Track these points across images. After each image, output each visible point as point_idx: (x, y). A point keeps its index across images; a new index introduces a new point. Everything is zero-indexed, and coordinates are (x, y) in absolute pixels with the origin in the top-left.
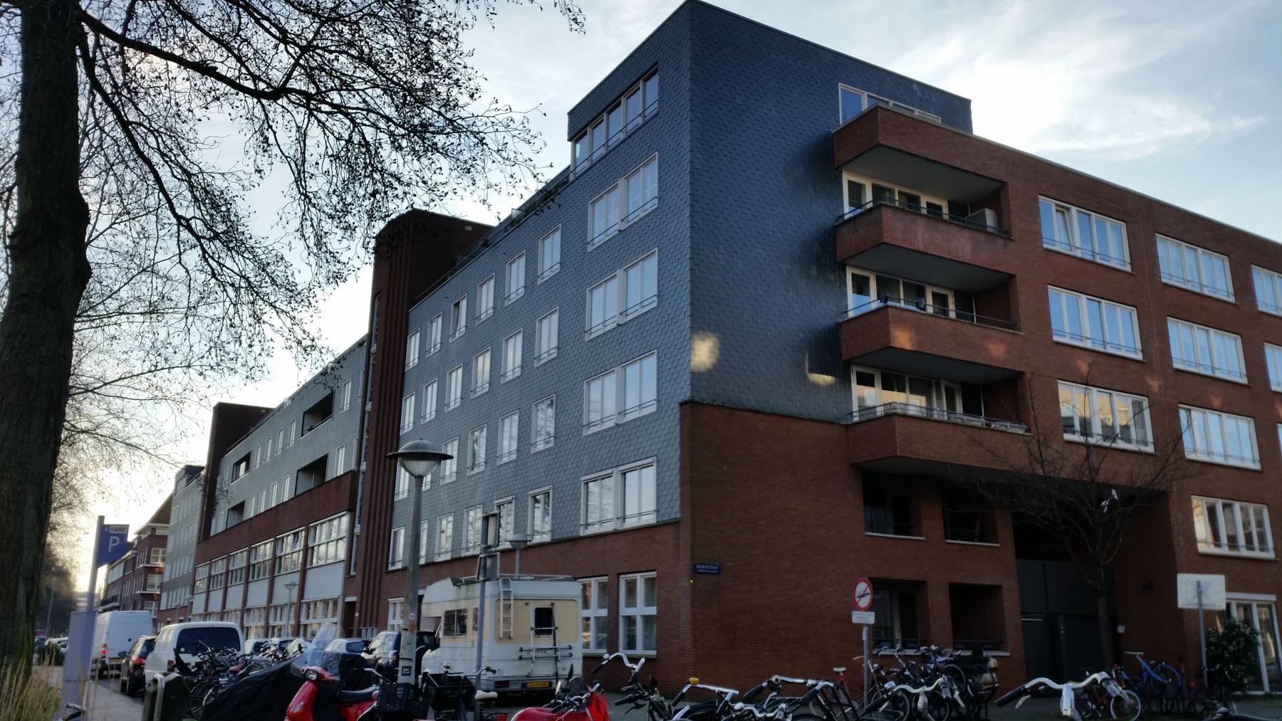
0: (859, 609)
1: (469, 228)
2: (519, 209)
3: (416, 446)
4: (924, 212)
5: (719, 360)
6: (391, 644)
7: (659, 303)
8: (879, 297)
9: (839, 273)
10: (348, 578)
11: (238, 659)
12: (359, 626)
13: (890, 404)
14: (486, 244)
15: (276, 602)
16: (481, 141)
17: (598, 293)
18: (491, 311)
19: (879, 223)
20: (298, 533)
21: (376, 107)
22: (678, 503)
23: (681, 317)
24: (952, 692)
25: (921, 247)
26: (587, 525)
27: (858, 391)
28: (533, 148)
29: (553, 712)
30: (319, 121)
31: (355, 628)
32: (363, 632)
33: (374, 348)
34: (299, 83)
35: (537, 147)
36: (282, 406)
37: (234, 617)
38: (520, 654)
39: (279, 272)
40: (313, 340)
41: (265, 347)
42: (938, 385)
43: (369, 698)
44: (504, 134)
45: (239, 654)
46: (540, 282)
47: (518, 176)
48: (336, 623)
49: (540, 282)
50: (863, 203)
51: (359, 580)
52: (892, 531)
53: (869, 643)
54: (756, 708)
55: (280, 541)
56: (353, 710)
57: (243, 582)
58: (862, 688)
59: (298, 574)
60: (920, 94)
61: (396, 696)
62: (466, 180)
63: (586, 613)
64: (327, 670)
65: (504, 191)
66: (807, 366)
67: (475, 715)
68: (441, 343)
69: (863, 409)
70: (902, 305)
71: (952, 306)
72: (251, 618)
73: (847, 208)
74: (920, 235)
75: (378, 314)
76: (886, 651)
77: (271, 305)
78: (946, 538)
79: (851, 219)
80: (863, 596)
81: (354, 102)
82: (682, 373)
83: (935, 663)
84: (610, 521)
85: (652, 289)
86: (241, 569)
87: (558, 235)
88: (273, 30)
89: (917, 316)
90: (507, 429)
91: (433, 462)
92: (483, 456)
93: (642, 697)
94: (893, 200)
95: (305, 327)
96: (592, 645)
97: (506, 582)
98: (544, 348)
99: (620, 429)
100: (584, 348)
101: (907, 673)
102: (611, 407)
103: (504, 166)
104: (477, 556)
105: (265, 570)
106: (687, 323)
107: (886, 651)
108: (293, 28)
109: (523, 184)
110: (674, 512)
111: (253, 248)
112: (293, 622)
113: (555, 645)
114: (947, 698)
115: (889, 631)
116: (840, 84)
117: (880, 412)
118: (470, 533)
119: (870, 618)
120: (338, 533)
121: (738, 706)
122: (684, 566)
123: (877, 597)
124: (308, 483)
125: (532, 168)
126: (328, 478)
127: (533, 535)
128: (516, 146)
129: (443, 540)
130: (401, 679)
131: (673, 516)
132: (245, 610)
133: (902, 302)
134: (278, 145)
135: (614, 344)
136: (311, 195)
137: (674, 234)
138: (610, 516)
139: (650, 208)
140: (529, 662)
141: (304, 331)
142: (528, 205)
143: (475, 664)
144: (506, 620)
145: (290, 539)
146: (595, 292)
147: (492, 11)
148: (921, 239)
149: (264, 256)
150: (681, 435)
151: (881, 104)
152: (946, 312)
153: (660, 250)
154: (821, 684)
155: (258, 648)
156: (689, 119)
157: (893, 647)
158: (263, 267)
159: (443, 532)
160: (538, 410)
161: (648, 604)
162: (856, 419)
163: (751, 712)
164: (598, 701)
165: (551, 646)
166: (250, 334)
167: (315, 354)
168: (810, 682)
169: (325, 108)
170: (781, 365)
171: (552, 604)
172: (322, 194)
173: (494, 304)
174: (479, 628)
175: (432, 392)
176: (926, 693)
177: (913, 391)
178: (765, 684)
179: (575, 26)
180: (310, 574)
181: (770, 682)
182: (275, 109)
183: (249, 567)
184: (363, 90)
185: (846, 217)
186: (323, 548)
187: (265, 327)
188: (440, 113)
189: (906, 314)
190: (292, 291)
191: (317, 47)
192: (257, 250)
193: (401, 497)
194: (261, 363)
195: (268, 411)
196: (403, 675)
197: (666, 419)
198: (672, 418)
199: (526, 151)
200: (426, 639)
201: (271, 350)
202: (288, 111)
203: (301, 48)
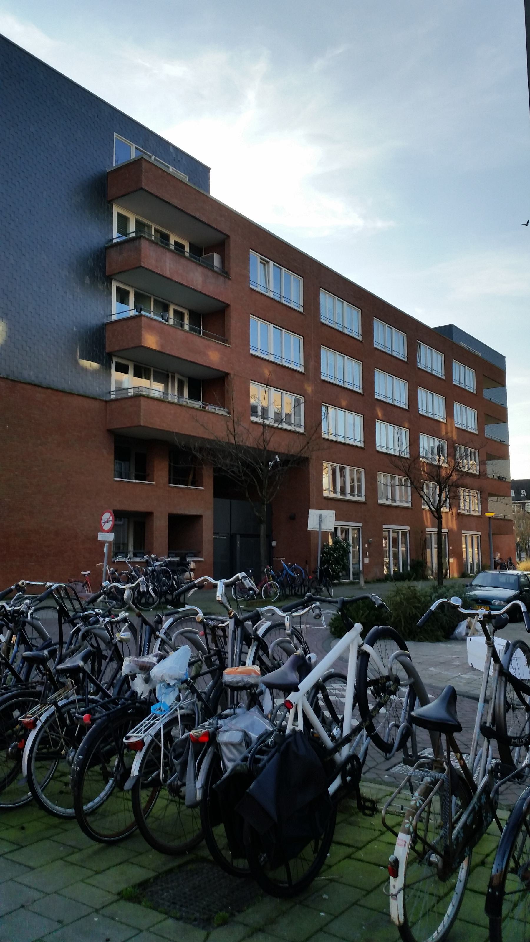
0: (104, 531)
4: (172, 247)
8: (136, 307)
9: (107, 285)
13: (139, 387)
19: (138, 250)
25: (168, 274)
27: (116, 375)
42: (173, 378)
52: (134, 478)
54: (8, 604)
60: (174, 156)
66: (78, 354)
69: (119, 389)
70: (152, 315)
73: (115, 234)
74: (168, 264)
76: (120, 559)
78: (170, 483)
79: (118, 244)
89: (162, 325)
94: (150, 235)
101: (133, 573)
107: (120, 559)
117: (131, 392)
119: (111, 537)
133: (152, 313)
148: (168, 268)
151: (145, 157)
152: (182, 326)
154: (56, 585)
162: (113, 397)
168: (48, 584)
176: (130, 588)
177: (156, 380)
178: (13, 587)
181: (18, 586)
189: (154, 323)
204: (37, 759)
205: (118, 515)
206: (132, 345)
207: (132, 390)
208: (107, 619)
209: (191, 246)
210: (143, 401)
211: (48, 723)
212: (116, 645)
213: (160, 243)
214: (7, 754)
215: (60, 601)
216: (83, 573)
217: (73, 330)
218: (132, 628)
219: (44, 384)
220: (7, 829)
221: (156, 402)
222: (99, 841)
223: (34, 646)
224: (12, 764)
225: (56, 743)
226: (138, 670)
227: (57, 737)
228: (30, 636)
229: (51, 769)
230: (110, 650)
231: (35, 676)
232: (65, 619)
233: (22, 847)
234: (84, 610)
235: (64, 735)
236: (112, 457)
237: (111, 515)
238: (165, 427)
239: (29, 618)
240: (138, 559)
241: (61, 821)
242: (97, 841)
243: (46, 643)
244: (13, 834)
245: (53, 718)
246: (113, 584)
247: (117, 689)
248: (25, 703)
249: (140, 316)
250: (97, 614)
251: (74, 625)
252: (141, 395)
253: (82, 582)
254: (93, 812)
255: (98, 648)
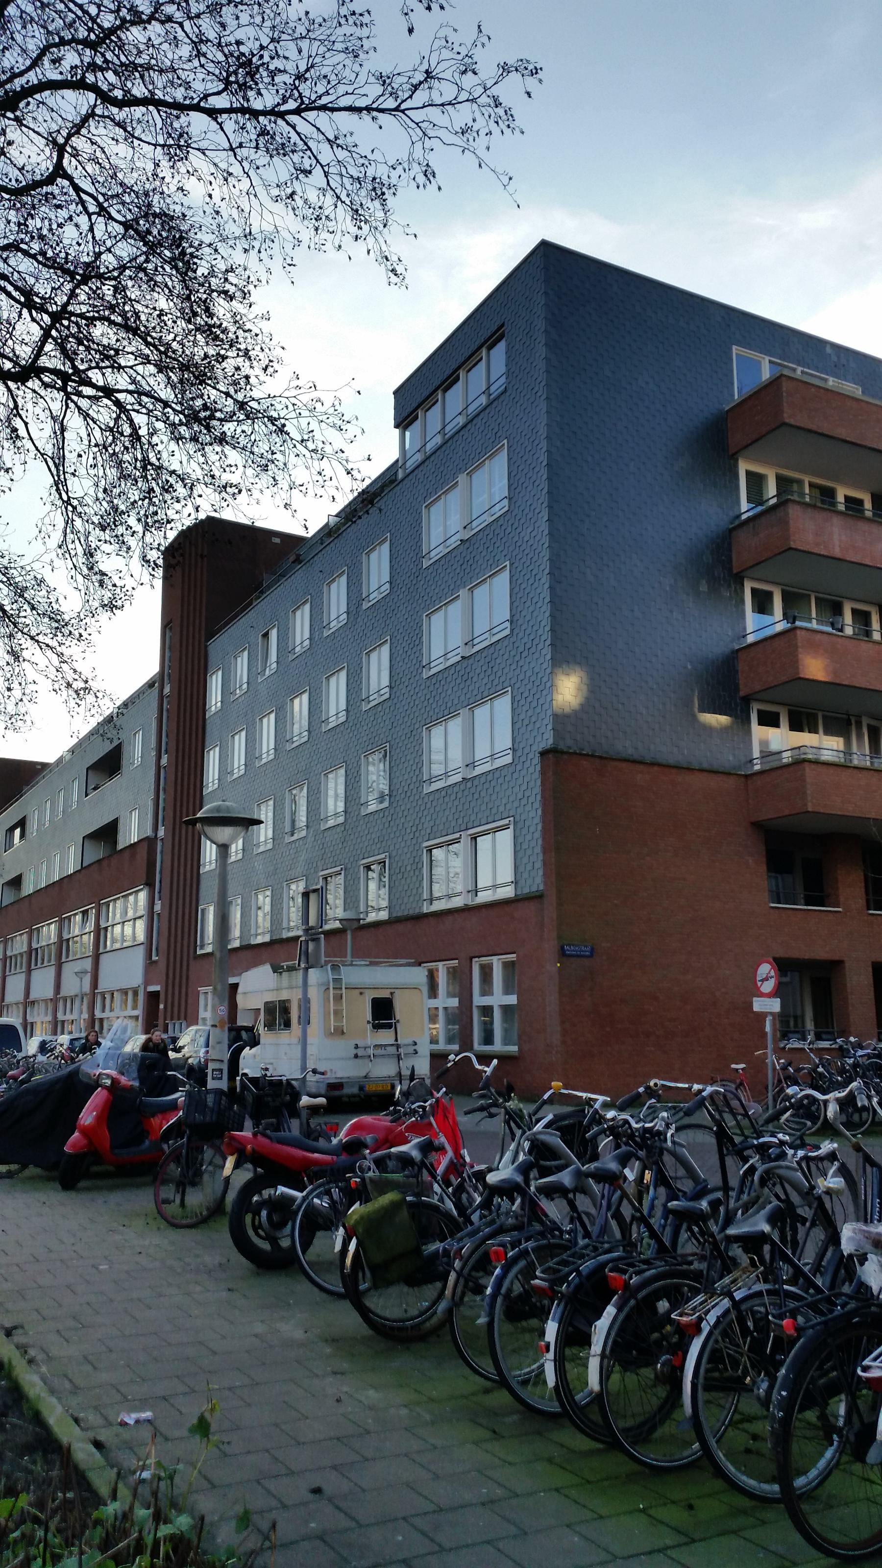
0: (762, 995)
1: (277, 540)
2: (336, 516)
3: (218, 809)
4: (841, 507)
5: (587, 699)
6: (202, 1040)
7: (512, 630)
8: (785, 616)
9: (736, 590)
10: (150, 964)
11: (18, 1062)
12: (165, 1019)
13: (799, 748)
14: (298, 560)
15: (64, 992)
16: (281, 430)
17: (437, 620)
18: (307, 643)
19: (784, 523)
20: (87, 910)
21: (148, 388)
22: (541, 873)
23: (540, 646)
24: (869, 1098)
25: (837, 552)
26: (431, 900)
27: (759, 732)
28: (346, 436)
29: (392, 1121)
30: (79, 408)
31: (161, 1021)
32: (170, 1027)
33: (167, 690)
34: (52, 359)
35: (349, 435)
36: (60, 760)
37: (15, 1012)
38: (355, 1051)
39: (39, 596)
40: (86, 682)
41: (27, 692)
42: (859, 725)
43: (173, 1106)
44: (310, 419)
45: (20, 1055)
46: (365, 605)
47: (328, 473)
48: (137, 1018)
49: (365, 605)
50: (765, 498)
51: (162, 965)
52: (802, 901)
53: (774, 1035)
54: (632, 1117)
55: (66, 921)
56: (155, 1121)
57: (53, 962)
58: (767, 1088)
59: (90, 959)
60: (834, 358)
61: (206, 1105)
62: (265, 479)
63: (433, 1003)
64: (123, 1074)
65: (311, 493)
66: (697, 705)
67: (301, 1124)
68: (248, 683)
69: (766, 754)
70: (814, 625)
71: (875, 624)
72: (35, 1013)
73: (744, 505)
74: (836, 537)
75: (170, 648)
76: (794, 1044)
77: (32, 638)
78: (869, 909)
79: (749, 520)
80: (766, 979)
81: (121, 381)
82: (542, 715)
83: (855, 1056)
84: (459, 894)
85: (503, 612)
86: (21, 954)
87: (386, 547)
88: (16, 294)
89: (834, 638)
90: (331, 785)
91: (239, 829)
92: (304, 819)
93: (495, 1105)
94: (802, 494)
95: (76, 665)
96: (442, 1039)
97: (335, 968)
98: (374, 687)
99: (469, 784)
100: (423, 687)
101: (820, 1069)
102: (456, 757)
103: (310, 461)
104: (299, 937)
105: (50, 956)
106: (547, 653)
107: (795, 1044)
108: (43, 289)
109: (334, 482)
110: (536, 882)
111: (6, 568)
112: (85, 1016)
113: (396, 1040)
114: (864, 1107)
115: (799, 1019)
116: (734, 347)
117: (787, 757)
118: (293, 909)
119: (775, 1005)
120: (135, 910)
121: (610, 1114)
122: (550, 947)
123: (785, 980)
124: (95, 853)
125: (344, 462)
126: (120, 846)
127: (367, 913)
128: (325, 434)
129: (260, 919)
130: (211, 1084)
131: (534, 889)
132: (28, 1003)
133: (814, 621)
134: (31, 439)
135: (458, 681)
136: (75, 503)
137: (530, 543)
138: (459, 888)
139: (498, 511)
140: (367, 1061)
141: (75, 671)
142: (348, 510)
143: (297, 1064)
144: (337, 1013)
145: (79, 918)
146: (434, 618)
147: (289, 261)
148: (837, 543)
149: (20, 579)
150: (543, 791)
151: (786, 372)
152: (868, 634)
153: (511, 565)
154: (709, 1089)
155: (43, 1048)
156: (544, 396)
157: (804, 1039)
158: (20, 592)
159: (260, 908)
160: (368, 764)
161: (507, 991)
162: (757, 768)
163: (626, 1122)
164: (445, 1110)
165: (392, 1042)
166: (9, 675)
167: (90, 698)
168: (696, 1087)
169: (88, 391)
170: (664, 704)
171: (392, 994)
172: (89, 500)
173: (311, 634)
174: (305, 1021)
175: (240, 742)
176: (838, 1100)
177: (828, 732)
178: (641, 1090)
179: (394, 279)
180: (104, 959)
181: (648, 1088)
182: (24, 394)
183: (31, 953)
184: (131, 367)
185: (744, 517)
186: (118, 929)
187: (25, 665)
188: (227, 394)
189: (818, 637)
190: (57, 621)
191: (72, 314)
192: (12, 571)
193: (207, 868)
194: (23, 711)
195: (44, 766)
196: (213, 1079)
197: (524, 772)
198: (531, 770)
199: (337, 440)
200: (244, 1035)
201: (35, 695)
202: (42, 397)
203: (51, 315)
204: (706, 1389)
205: (783, 965)
206: (784, 679)
207: (788, 754)
208: (801, 1153)
209: (875, 498)
210: (808, 769)
211: (721, 1327)
212: (819, 1199)
213: (819, 504)
214: (656, 1374)
215: (717, 1117)
216: (733, 1066)
217: (686, 667)
218: (843, 1171)
219: (648, 759)
220: (665, 1504)
221: (831, 770)
222: (829, 1553)
223: (679, 1190)
224: (662, 1392)
225: (735, 1364)
226: (868, 1247)
227: (736, 1352)
228: (672, 1174)
229: (728, 1406)
230: (810, 1207)
231: (688, 1246)
232: (727, 1149)
233: (694, 1541)
234: (759, 1135)
235: (749, 1350)
236: (763, 868)
237: (773, 968)
238: (850, 810)
239: (669, 1143)
240: (825, 1044)
241: (753, 1503)
242: (822, 1552)
243: (699, 1187)
244: (675, 1515)
245: (728, 1319)
246: (804, 1093)
247: (828, 1278)
248: (677, 1288)
249: (796, 628)
250: (782, 1143)
251: (745, 1160)
252: (804, 761)
253: (735, 1082)
254: (809, 1495)
255: (788, 1201)
